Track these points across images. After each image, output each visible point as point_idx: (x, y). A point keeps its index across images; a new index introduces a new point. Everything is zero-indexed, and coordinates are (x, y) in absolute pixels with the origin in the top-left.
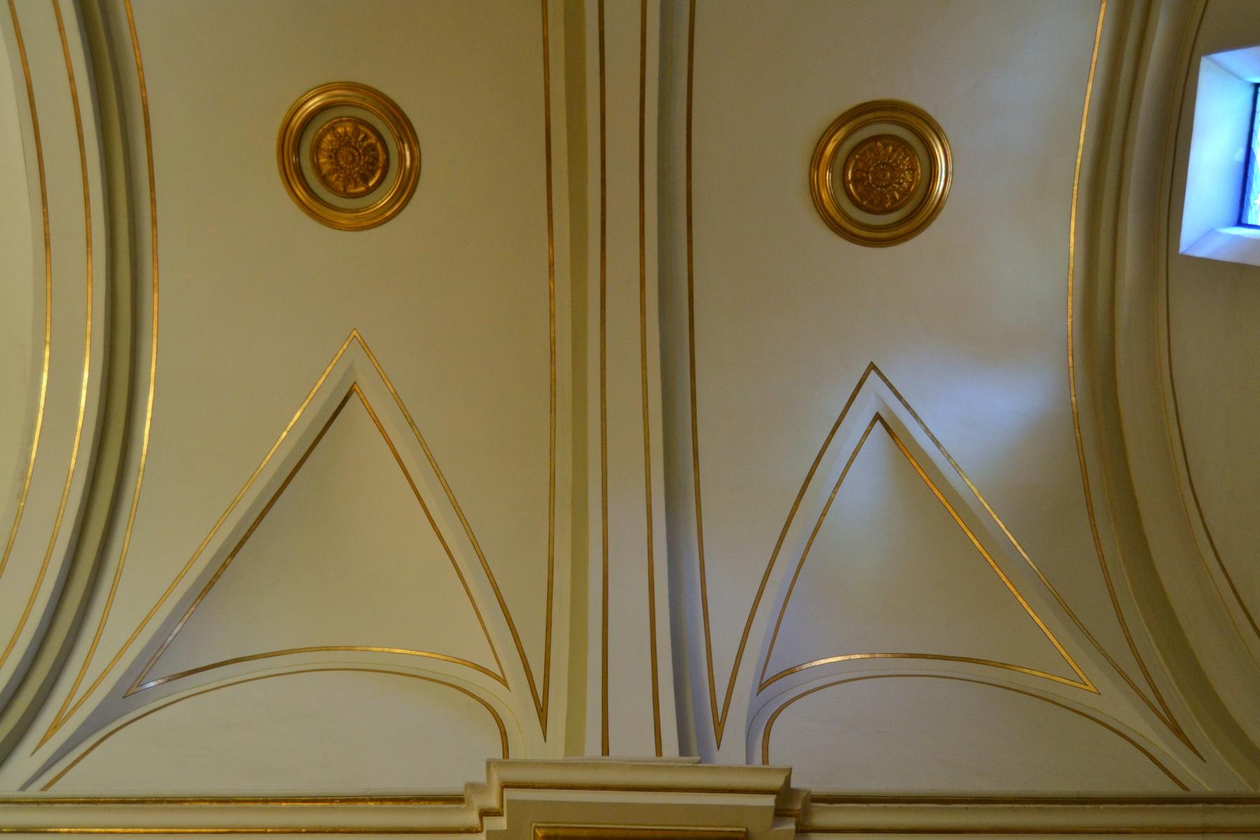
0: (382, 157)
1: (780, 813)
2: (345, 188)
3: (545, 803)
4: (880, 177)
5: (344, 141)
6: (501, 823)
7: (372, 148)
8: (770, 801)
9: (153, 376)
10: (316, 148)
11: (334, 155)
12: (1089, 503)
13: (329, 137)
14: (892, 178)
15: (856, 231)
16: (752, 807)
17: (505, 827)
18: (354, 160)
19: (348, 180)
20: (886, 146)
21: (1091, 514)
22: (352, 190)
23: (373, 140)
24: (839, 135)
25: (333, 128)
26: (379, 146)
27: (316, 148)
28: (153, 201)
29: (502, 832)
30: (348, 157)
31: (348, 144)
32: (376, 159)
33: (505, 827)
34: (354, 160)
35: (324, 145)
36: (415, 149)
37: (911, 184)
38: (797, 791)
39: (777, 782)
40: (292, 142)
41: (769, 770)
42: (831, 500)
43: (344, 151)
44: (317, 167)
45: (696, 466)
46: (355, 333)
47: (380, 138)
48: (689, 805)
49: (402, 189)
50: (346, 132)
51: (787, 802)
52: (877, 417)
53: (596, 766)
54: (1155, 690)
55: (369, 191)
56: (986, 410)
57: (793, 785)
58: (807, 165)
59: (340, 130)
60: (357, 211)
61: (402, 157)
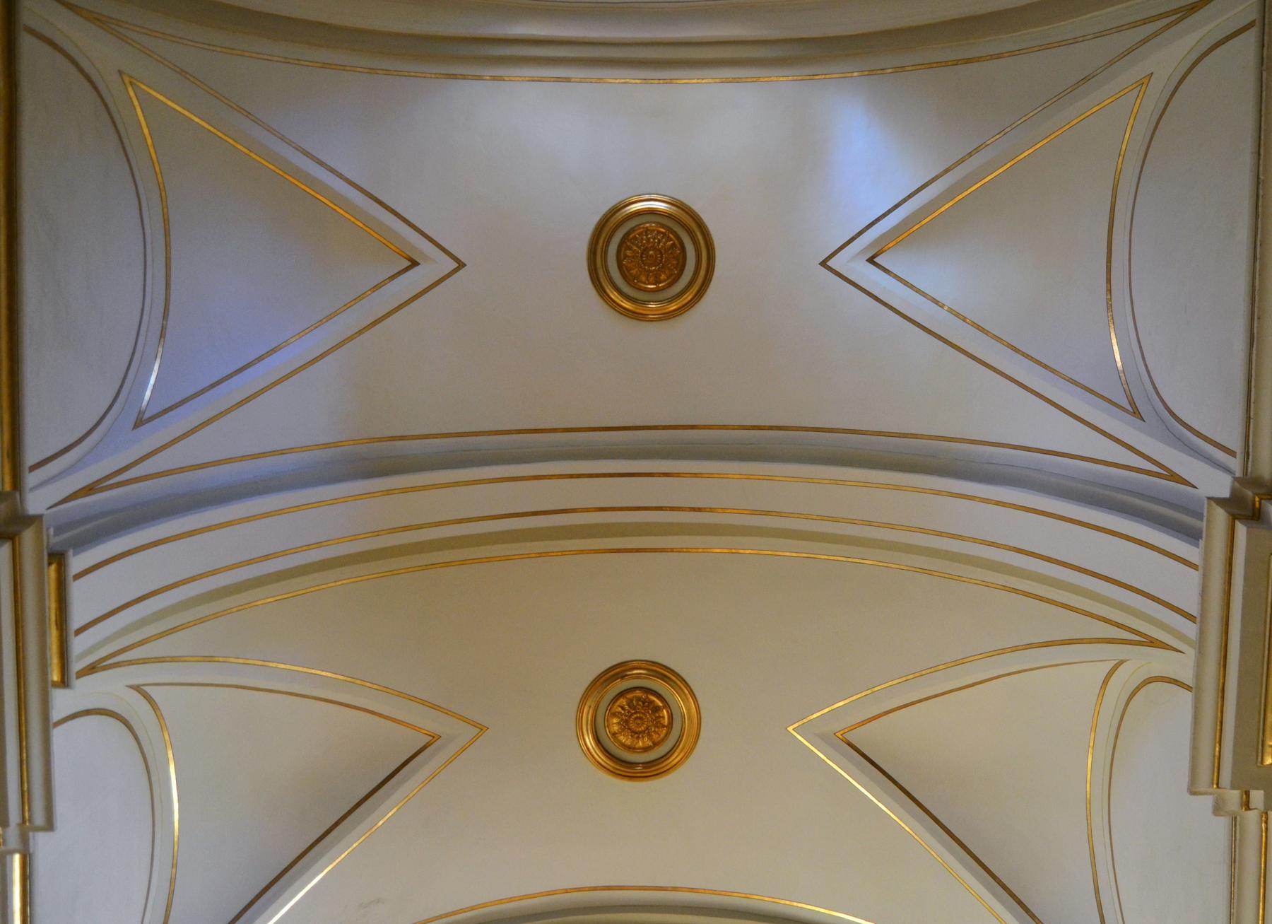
0: (638, 693)
1: (1255, 516)
2: (663, 726)
3: (1246, 578)
4: (652, 258)
5: (625, 724)
6: (1257, 797)
7: (630, 703)
8: (1241, 530)
9: (827, 912)
10: (630, 748)
11: (636, 734)
12: (957, 63)
13: (622, 738)
14: (654, 248)
15: (702, 273)
16: (1236, 733)
17: (1262, 792)
18: (640, 718)
19: (657, 723)
20: (626, 256)
21: (968, 61)
22: (666, 722)
23: (623, 701)
24: (614, 295)
25: (614, 734)
26: (629, 696)
27: (630, 748)
28: (675, 889)
29: (1267, 797)
30: (639, 721)
31: (627, 722)
32: (639, 699)
33: (1262, 792)
34: (640, 718)
35: (628, 743)
36: (635, 664)
37: (659, 232)
38: (1233, 491)
39: (1221, 516)
40: (624, 768)
41: (1202, 616)
42: (951, 311)
43: (632, 726)
44: (646, 749)
45: (914, 436)
46: (790, 729)
47: (622, 694)
48: (1241, 647)
49: (664, 677)
50: (619, 723)
51: (1245, 506)
52: (871, 260)
53: (1205, 577)
54: (1146, 21)
55: (666, 705)
56: (861, 155)
57: (1226, 493)
58: (643, 324)
59: (616, 728)
60: (681, 736)
61: (638, 676)
